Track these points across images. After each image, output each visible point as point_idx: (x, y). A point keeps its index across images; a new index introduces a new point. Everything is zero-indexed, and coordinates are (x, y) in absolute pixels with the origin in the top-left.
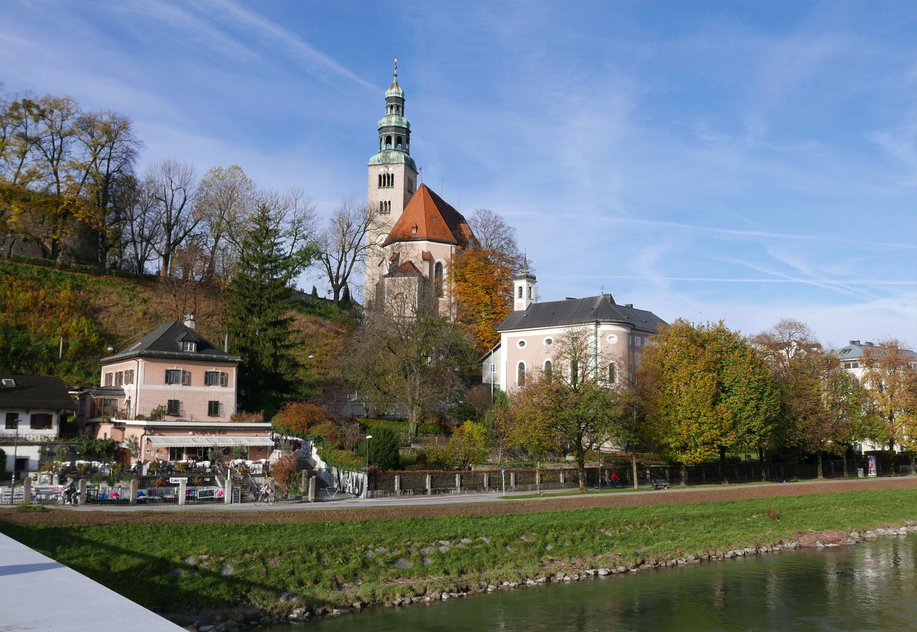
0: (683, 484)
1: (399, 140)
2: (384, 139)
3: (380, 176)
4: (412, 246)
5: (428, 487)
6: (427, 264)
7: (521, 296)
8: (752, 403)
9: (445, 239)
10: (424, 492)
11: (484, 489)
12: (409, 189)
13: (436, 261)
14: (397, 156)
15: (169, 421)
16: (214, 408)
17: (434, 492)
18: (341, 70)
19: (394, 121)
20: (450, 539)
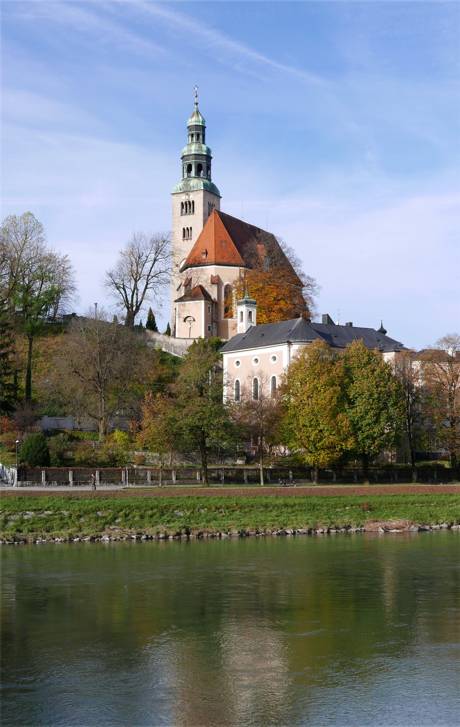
0: (314, 483)
1: (199, 168)
2: (186, 167)
3: (182, 203)
4: (203, 270)
5: (71, 479)
6: (215, 288)
7: (242, 320)
8: (372, 413)
9: (233, 262)
10: (67, 483)
11: (122, 483)
12: (207, 215)
13: (225, 284)
14: (197, 183)
17: (75, 484)
18: (255, 56)
19: (194, 149)
20: (35, 510)
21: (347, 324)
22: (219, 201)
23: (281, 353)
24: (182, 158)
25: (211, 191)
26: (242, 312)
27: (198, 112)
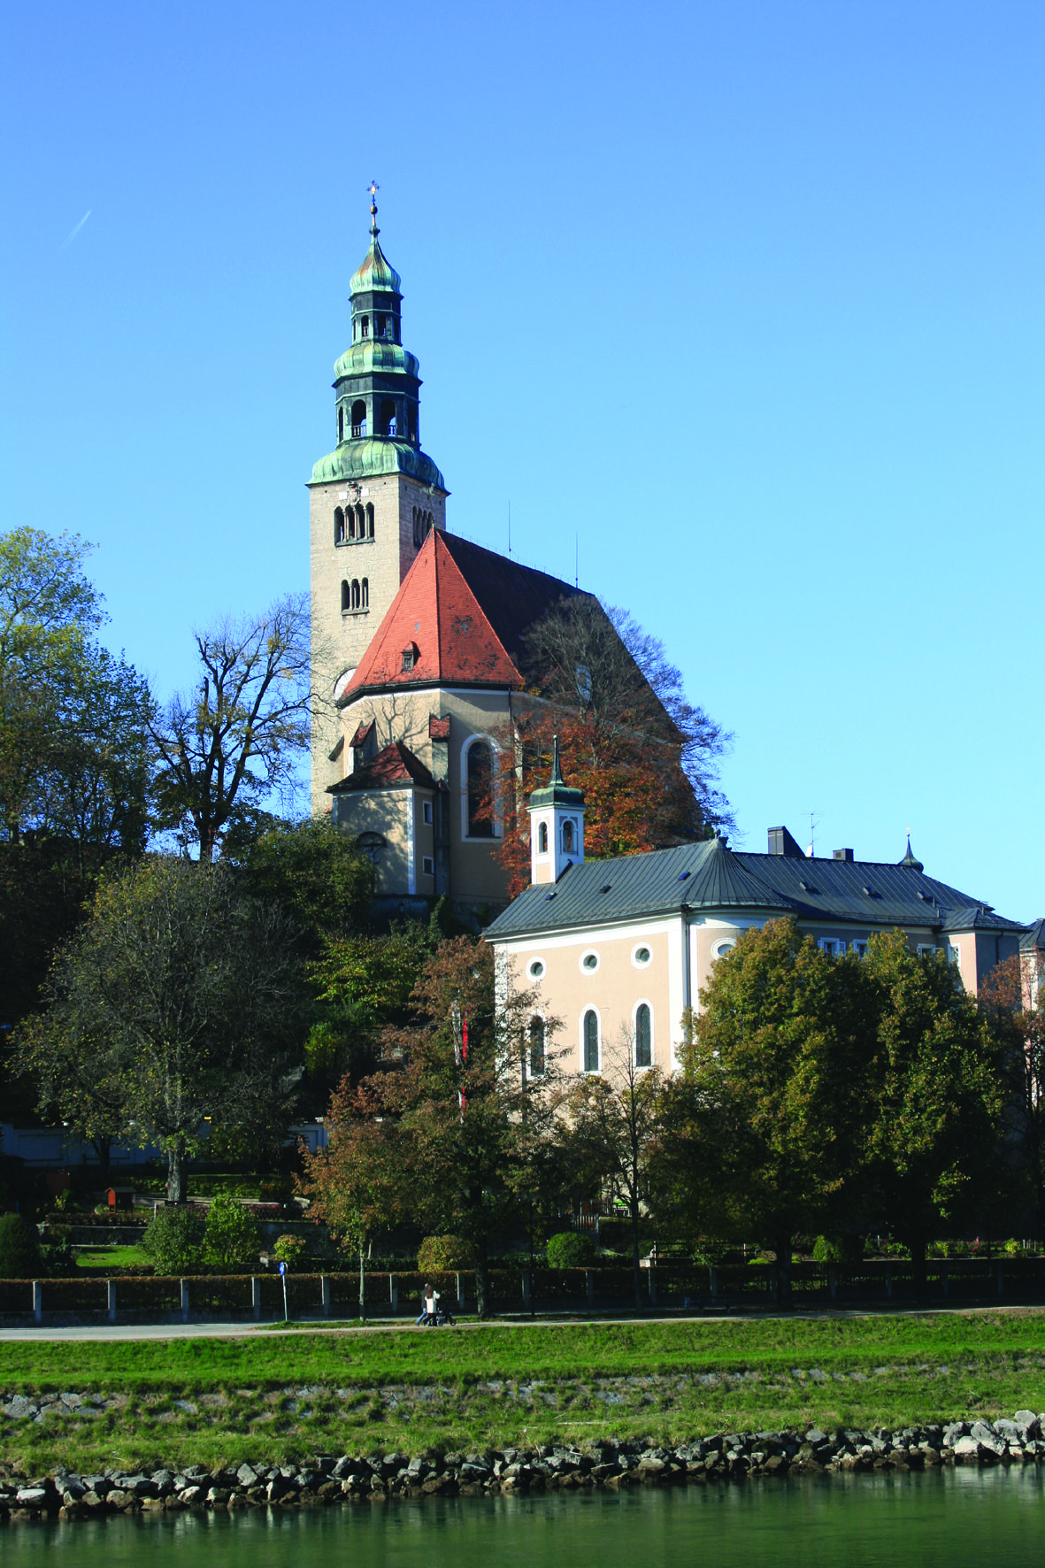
2: (347, 409)
3: (338, 512)
12: (411, 544)
14: (382, 456)
21: (837, 853)
22: (442, 504)
23: (663, 939)
24: (336, 385)
25: (419, 474)
26: (543, 827)
27: (379, 256)
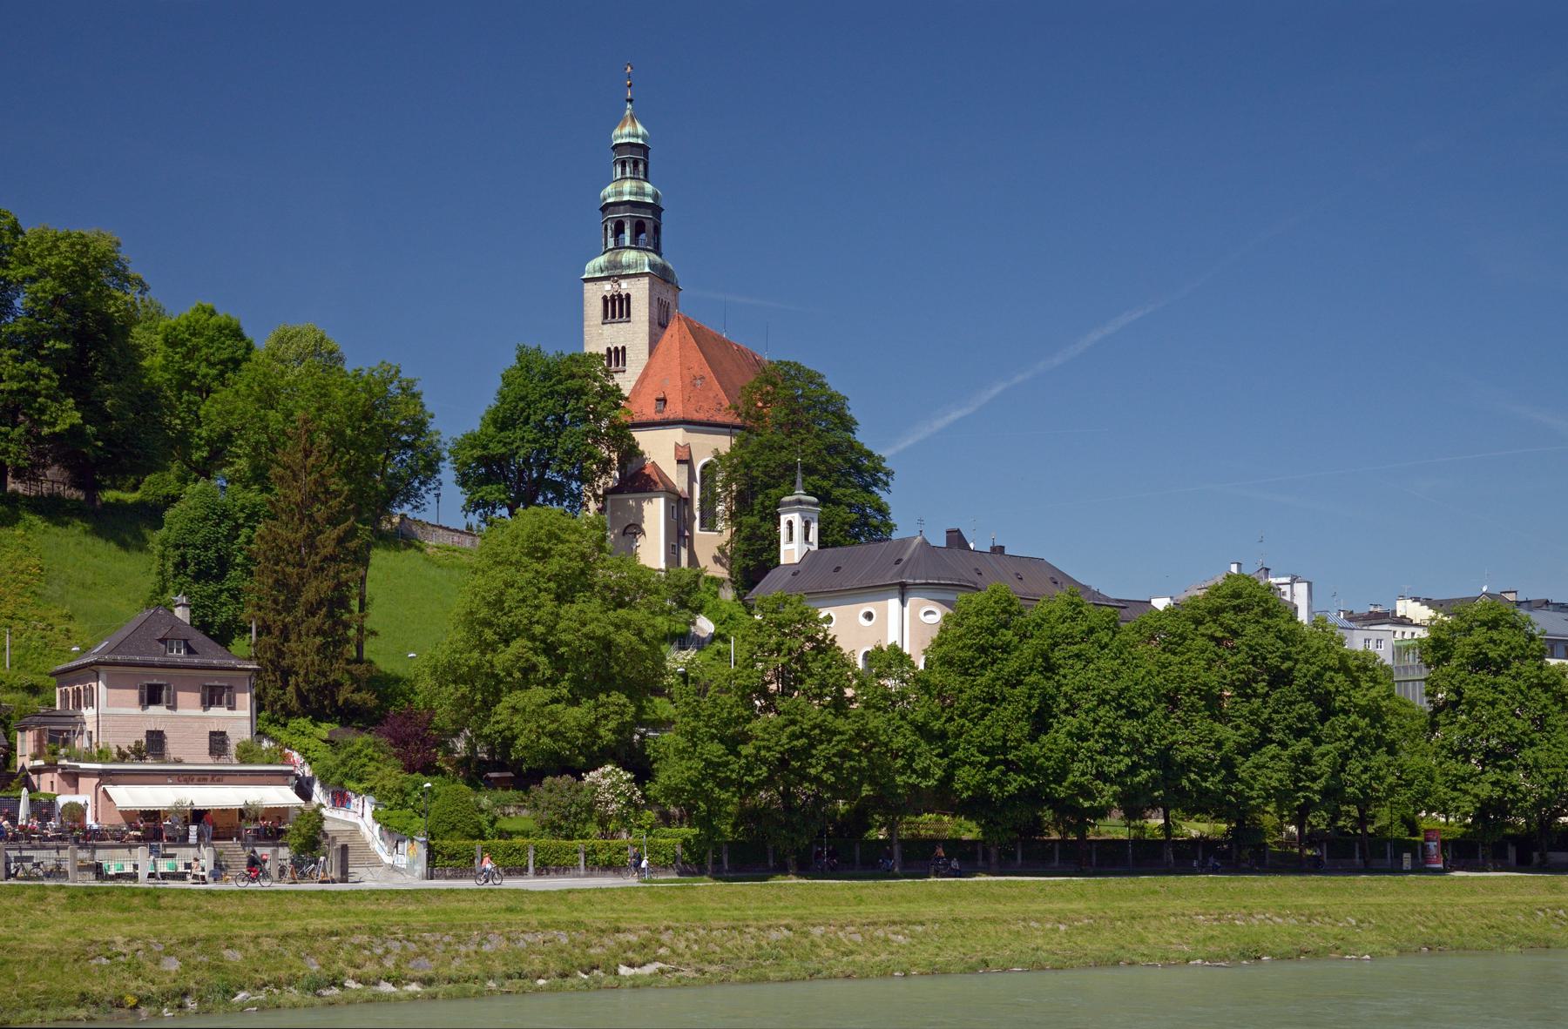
3: (605, 298)
12: (660, 323)
15: (150, 765)
16: (218, 742)
17: (538, 873)
26: (790, 523)
